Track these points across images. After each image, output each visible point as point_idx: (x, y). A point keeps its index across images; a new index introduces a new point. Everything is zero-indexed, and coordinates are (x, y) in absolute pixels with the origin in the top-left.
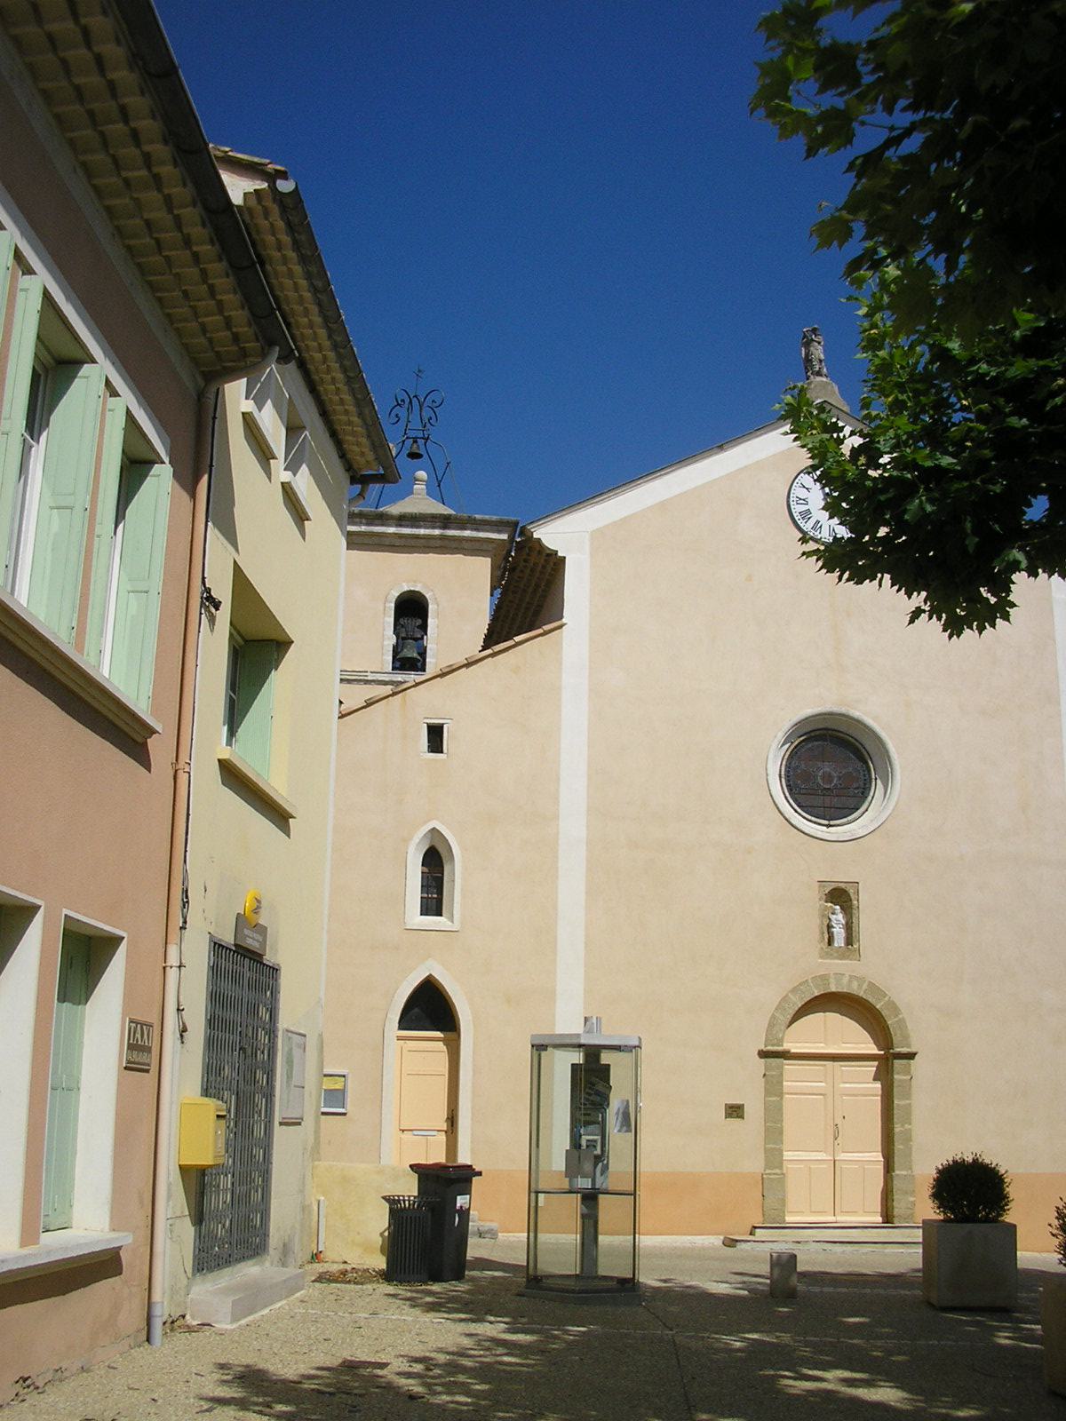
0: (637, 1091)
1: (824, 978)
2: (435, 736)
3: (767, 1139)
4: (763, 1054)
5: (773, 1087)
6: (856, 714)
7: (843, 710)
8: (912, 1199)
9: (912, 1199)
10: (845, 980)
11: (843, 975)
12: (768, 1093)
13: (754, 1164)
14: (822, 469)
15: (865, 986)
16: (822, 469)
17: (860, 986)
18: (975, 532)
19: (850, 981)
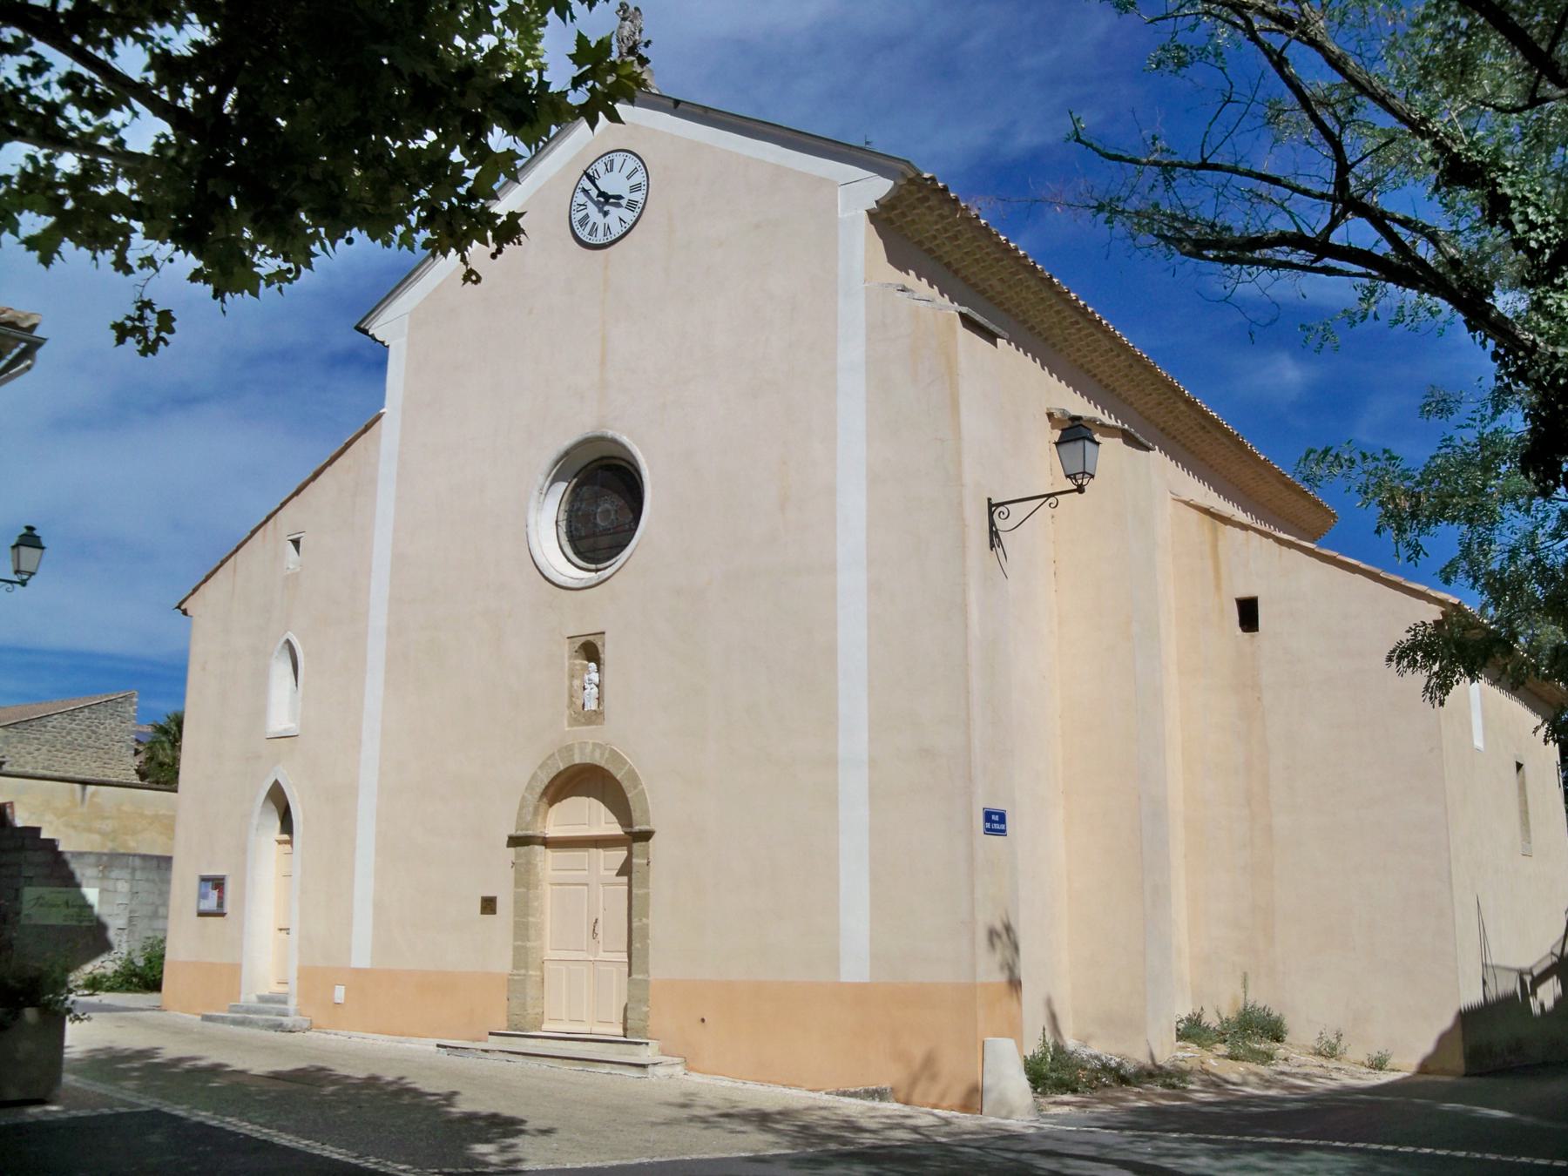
0: (1215, 547)
1: (569, 748)
2: (604, 494)
3: (517, 936)
4: (515, 841)
5: (525, 878)
6: (610, 433)
7: (598, 433)
8: (645, 1009)
9: (645, 1009)
10: (589, 749)
11: (587, 747)
12: (517, 884)
13: (503, 964)
14: (89, 48)
15: (607, 755)
16: (89, 48)
17: (602, 755)
18: (96, 48)
19: (593, 751)
